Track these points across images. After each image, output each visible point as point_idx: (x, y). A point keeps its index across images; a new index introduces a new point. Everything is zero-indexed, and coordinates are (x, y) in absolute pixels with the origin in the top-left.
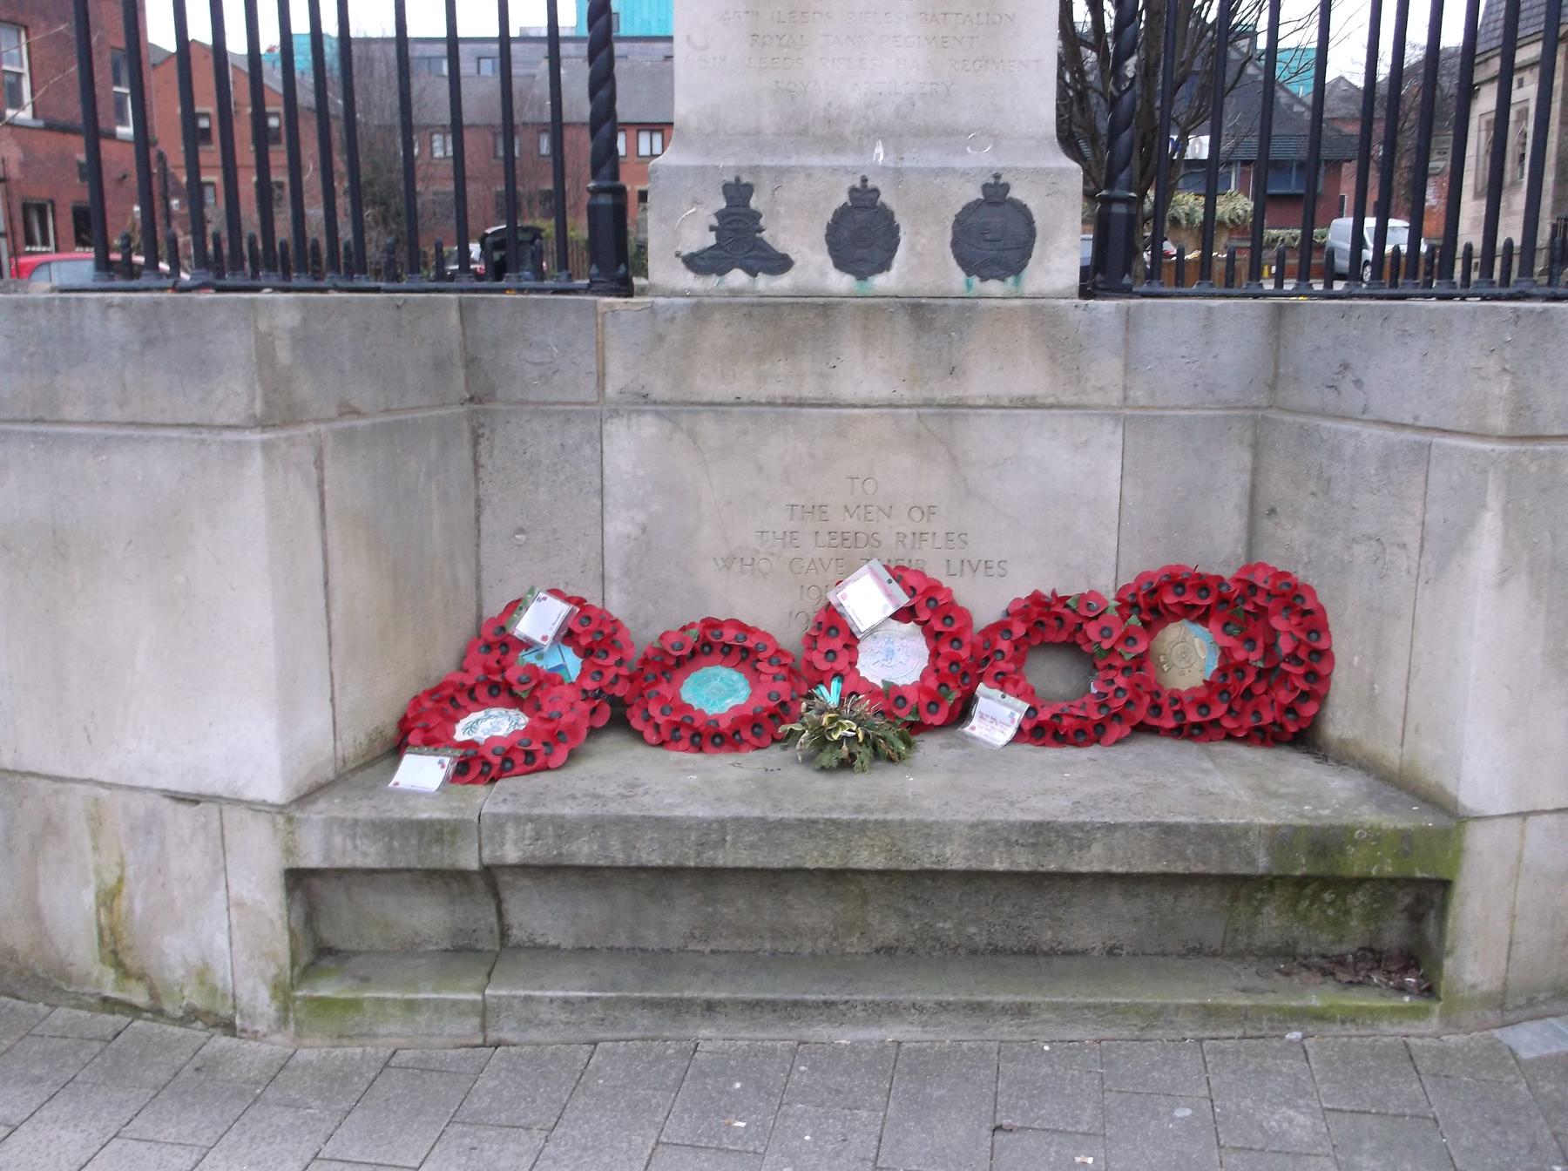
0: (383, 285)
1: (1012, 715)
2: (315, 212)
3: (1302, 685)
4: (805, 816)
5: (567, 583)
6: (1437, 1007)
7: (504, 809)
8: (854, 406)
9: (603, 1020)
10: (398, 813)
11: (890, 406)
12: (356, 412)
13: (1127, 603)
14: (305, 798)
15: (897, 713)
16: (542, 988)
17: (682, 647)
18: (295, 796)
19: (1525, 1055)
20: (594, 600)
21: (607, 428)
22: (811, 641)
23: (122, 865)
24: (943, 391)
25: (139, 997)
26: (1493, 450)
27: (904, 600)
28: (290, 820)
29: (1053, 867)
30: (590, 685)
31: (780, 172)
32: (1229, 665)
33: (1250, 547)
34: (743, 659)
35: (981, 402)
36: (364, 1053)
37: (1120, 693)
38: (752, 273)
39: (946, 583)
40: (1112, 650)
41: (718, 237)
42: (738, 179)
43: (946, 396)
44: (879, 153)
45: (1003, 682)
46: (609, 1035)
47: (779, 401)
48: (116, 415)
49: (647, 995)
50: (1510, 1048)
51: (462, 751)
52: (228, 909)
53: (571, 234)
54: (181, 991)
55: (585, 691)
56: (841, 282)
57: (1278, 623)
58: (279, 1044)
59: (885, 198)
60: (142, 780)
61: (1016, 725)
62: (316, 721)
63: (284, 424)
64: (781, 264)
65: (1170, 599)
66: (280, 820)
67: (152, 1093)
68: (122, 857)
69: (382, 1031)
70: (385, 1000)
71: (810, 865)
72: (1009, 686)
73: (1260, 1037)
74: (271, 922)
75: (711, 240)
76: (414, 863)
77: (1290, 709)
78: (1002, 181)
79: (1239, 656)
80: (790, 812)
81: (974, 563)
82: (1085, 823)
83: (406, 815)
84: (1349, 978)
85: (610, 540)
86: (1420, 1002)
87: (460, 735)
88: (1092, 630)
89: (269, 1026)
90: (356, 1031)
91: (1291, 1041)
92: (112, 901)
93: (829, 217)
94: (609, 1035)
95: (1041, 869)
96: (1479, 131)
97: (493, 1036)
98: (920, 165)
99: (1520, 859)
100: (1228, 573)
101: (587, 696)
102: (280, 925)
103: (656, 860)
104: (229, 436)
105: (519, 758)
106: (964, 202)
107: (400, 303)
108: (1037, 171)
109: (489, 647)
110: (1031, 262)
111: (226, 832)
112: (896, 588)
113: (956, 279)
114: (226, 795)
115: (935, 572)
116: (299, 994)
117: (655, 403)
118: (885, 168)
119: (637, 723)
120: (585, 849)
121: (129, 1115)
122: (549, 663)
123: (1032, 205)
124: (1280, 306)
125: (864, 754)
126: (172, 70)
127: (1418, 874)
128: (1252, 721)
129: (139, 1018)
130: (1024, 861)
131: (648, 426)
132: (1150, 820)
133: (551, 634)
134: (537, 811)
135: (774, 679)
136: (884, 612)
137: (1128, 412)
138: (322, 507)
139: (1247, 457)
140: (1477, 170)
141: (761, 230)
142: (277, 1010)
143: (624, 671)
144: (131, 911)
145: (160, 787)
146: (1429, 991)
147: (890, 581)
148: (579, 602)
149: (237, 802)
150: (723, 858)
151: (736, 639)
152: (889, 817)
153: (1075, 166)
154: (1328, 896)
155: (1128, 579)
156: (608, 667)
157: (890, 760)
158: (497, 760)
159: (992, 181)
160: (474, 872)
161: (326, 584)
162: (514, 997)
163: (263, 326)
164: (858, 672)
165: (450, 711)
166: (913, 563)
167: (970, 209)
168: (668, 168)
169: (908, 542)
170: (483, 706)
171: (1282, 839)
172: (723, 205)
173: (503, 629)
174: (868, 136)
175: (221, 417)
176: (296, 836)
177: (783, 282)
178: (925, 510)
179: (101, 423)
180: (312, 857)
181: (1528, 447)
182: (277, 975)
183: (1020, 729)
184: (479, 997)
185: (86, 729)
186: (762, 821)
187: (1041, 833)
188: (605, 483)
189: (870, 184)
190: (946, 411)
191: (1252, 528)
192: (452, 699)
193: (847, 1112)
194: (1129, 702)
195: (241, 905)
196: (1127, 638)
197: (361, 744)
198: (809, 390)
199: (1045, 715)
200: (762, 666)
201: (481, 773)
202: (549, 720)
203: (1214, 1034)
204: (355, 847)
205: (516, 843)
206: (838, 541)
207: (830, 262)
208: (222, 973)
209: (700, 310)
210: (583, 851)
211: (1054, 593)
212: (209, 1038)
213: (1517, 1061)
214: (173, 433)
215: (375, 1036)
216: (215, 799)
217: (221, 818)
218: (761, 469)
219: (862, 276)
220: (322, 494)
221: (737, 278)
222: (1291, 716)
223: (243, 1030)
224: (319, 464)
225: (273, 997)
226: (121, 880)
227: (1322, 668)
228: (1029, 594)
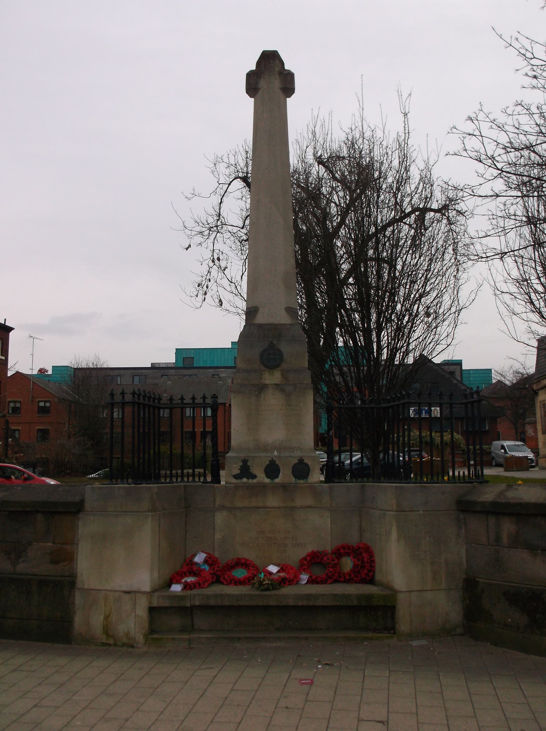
6: (395, 636)
13: (333, 553)
14: (154, 591)
17: (232, 564)
25: (111, 641)
28: (151, 596)
29: (311, 604)
30: (212, 572)
32: (355, 566)
35: (299, 507)
38: (248, 479)
40: (329, 563)
42: (245, 459)
44: (276, 453)
53: (174, 451)
56: (267, 481)
57: (364, 555)
58: (145, 649)
59: (277, 462)
60: (118, 589)
62: (156, 575)
64: (254, 477)
65: (342, 551)
66: (149, 596)
71: (260, 604)
75: (239, 472)
79: (356, 563)
88: (325, 559)
96: (541, 408)
97: (192, 646)
101: (211, 574)
104: (144, 513)
105: (197, 585)
106: (294, 463)
110: (309, 476)
113: (293, 480)
114: (137, 590)
118: (277, 456)
122: (203, 567)
124: (363, 485)
125: (271, 587)
130: (305, 603)
131: (225, 513)
133: (202, 561)
140: (542, 422)
141: (250, 470)
143: (219, 569)
148: (209, 554)
149: (139, 592)
150: (242, 603)
159: (300, 458)
167: (295, 465)
171: (360, 597)
173: (191, 560)
177: (255, 481)
180: (155, 604)
183: (308, 580)
187: (308, 597)
189: (274, 459)
194: (333, 574)
196: (333, 560)
198: (260, 504)
199: (314, 577)
200: (251, 568)
209: (237, 487)
210: (212, 602)
216: (135, 592)
220: (160, 526)
221: (245, 480)
223: (136, 647)
224: (160, 520)
226: (110, 613)
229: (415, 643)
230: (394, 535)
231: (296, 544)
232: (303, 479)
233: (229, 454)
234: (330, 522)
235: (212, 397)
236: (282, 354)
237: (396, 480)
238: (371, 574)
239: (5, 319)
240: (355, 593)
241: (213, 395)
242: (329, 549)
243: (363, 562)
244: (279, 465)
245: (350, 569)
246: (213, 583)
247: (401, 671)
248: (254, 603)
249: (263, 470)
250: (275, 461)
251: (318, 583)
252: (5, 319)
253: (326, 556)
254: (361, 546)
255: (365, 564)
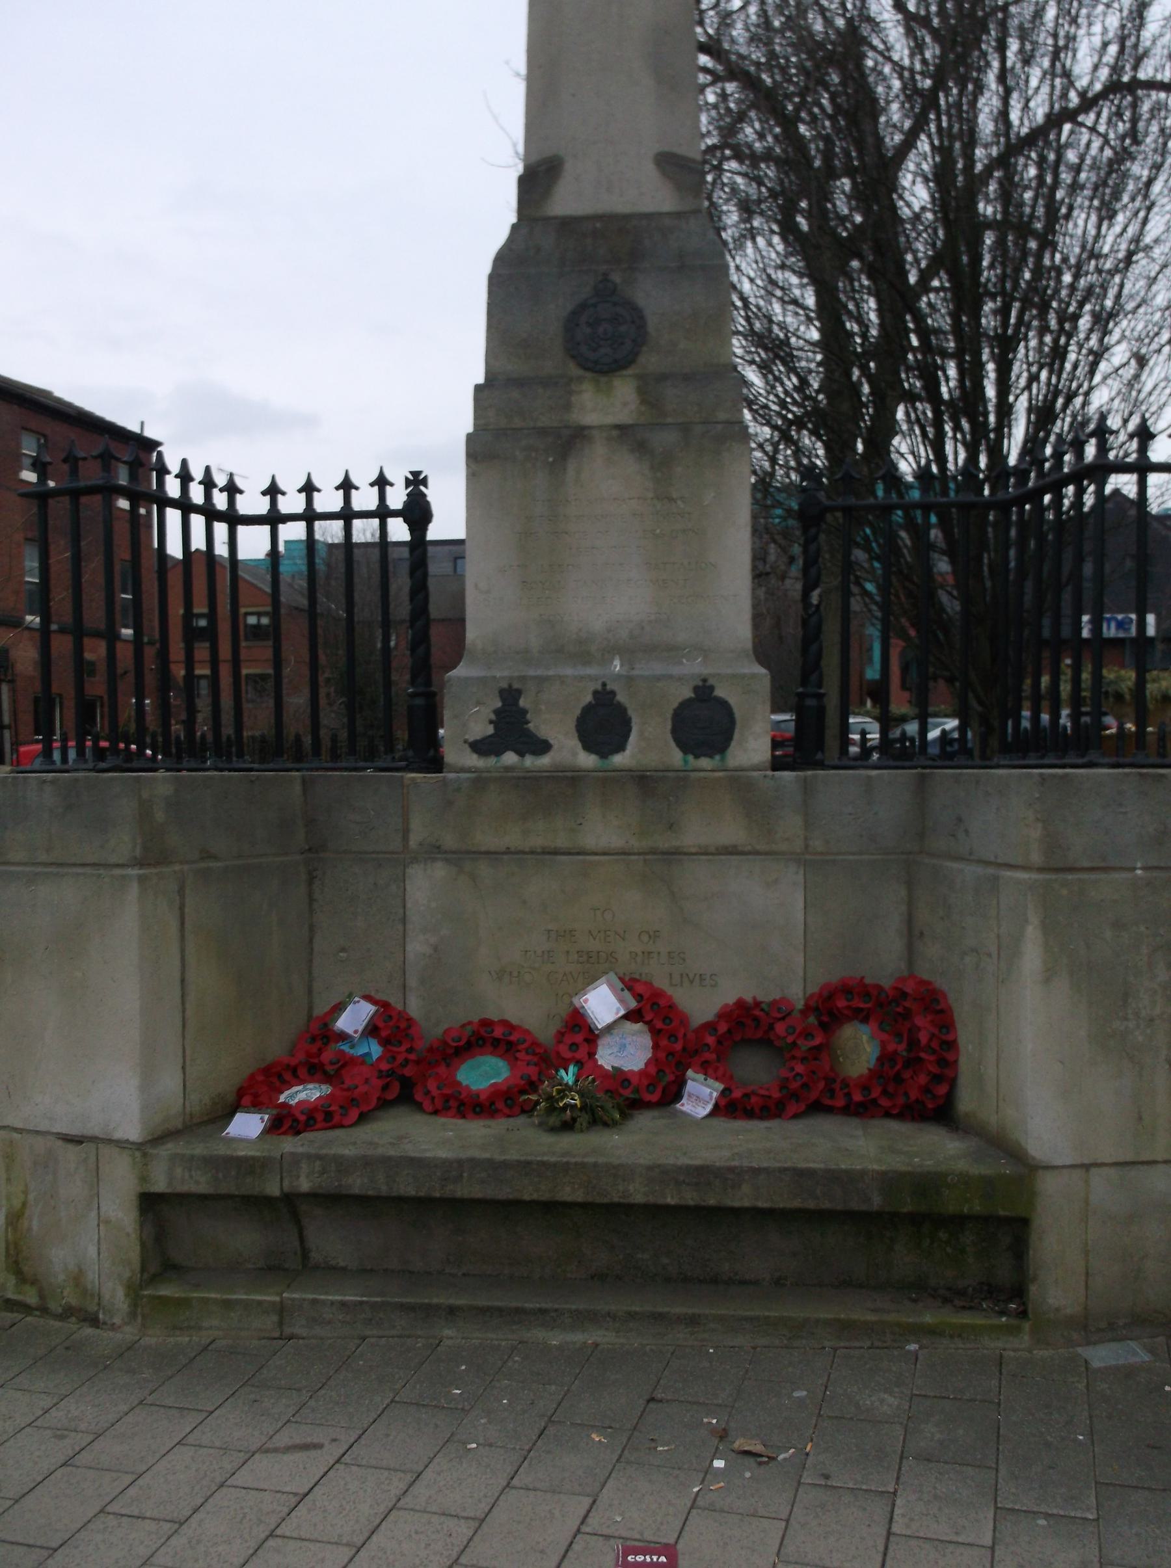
0: (256, 766)
1: (711, 1094)
2: (297, 701)
3: (934, 1069)
4: (522, 1158)
5: (377, 990)
6: (1027, 1326)
7: (300, 1150)
8: (596, 854)
9: (371, 1320)
10: (222, 1150)
11: (625, 853)
12: (214, 857)
13: (808, 1009)
14: (158, 1139)
15: (621, 1091)
16: (326, 1293)
18: (150, 1138)
19: (1096, 1364)
20: (396, 1002)
21: (409, 871)
22: (560, 1035)
23: (26, 1193)
24: (664, 842)
25: (31, 1298)
26: (1030, 879)
27: (633, 1004)
28: (145, 1155)
29: (712, 1202)
31: (541, 680)
32: (885, 1058)
33: (910, 963)
34: (507, 1051)
35: (693, 850)
36: (190, 1341)
37: (798, 1078)
38: (522, 754)
39: (670, 991)
40: (794, 1043)
41: (495, 728)
42: (510, 686)
43: (666, 846)
44: (617, 666)
45: (706, 1069)
46: (375, 1332)
47: (539, 850)
48: (43, 857)
49: (404, 1300)
50: (1086, 1361)
51: (278, 1110)
52: (98, 1225)
54: (62, 1292)
55: (381, 1071)
56: (587, 760)
57: (920, 1021)
58: (129, 1333)
59: (621, 698)
61: (713, 1101)
62: (170, 1083)
63: (157, 864)
64: (543, 747)
65: (841, 1003)
66: (138, 1154)
67: (31, 1362)
68: (26, 1186)
69: (205, 1324)
70: (208, 1299)
71: (526, 1197)
72: (710, 1071)
73: (883, 1348)
74: (128, 1235)
75: (490, 730)
76: (233, 1190)
77: (926, 1090)
78: (707, 684)
79: (891, 1047)
80: (513, 1155)
81: (691, 976)
82: (736, 1167)
83: (229, 1153)
84: (962, 1304)
85: (410, 956)
86: (1014, 1322)
87: (282, 1098)
88: (780, 1028)
89: (123, 1319)
90: (186, 1324)
91: (909, 1351)
92: (18, 1220)
93: (578, 712)
94: (375, 1332)
95: (703, 1204)
97: (288, 1331)
98: (647, 673)
99: (1087, 1202)
100: (887, 983)
101: (381, 1075)
102: (134, 1236)
103: (411, 1191)
104: (118, 872)
105: (320, 1117)
106: (680, 700)
107: (253, 779)
108: (734, 676)
109: (314, 1039)
110: (733, 744)
111: (100, 1165)
112: (627, 995)
113: (676, 757)
114: (101, 1136)
115: (661, 983)
116: (146, 1293)
117: (446, 852)
118: (619, 677)
119: (418, 1097)
120: (359, 1181)
121: (12, 1375)
122: (361, 1050)
123: (732, 701)
124: (923, 775)
125: (584, 1119)
126: (179, 570)
127: (1002, 1213)
128: (902, 1100)
129: (31, 1315)
130: (690, 1197)
131: (440, 871)
132: (786, 1165)
133: (361, 1029)
134: (324, 1152)
135: (528, 1064)
136: (617, 1013)
137: (808, 857)
138: (182, 924)
139: (903, 892)
141: (528, 722)
142: (129, 1306)
143: (412, 1057)
144: (29, 1229)
145: (55, 1131)
146: (1023, 1314)
147: (622, 990)
149: (110, 1141)
151: (503, 1034)
152: (586, 1160)
153: (763, 671)
154: (943, 1235)
155: (813, 989)
156: (399, 1053)
157: (606, 1125)
158: (303, 1118)
159: (700, 684)
160: (276, 1198)
161: (183, 981)
162: (304, 1300)
163: (145, 795)
164: (596, 1061)
165: (278, 1084)
166: (644, 976)
167: (685, 705)
168: (459, 678)
169: (639, 959)
170: (302, 1082)
171: (890, 1182)
172: (499, 704)
173: (326, 1025)
174: (609, 652)
175: (114, 859)
176: (149, 1167)
177: (545, 761)
178: (651, 933)
179: (34, 864)
180: (160, 1185)
181: (1061, 876)
182: (131, 1278)
184: (277, 1299)
185: (7, 1088)
186: (490, 1162)
187: (702, 1175)
188: (408, 913)
189: (608, 687)
190: (665, 857)
191: (910, 948)
192: (280, 1076)
193: (541, 1386)
194: (804, 1085)
195: (107, 1222)
196: (807, 1034)
197: (205, 1104)
198: (561, 842)
199: (737, 1094)
200: (520, 1055)
201: (291, 1127)
202: (348, 1090)
203: (847, 1344)
204: (191, 1177)
205: (307, 1177)
206: (585, 958)
207: (580, 746)
208: (92, 1277)
209: (480, 782)
210: (357, 1184)
211: (754, 998)
212: (79, 1329)
213: (1087, 1369)
214: (80, 870)
215: (200, 1328)
216: (93, 1139)
217: (97, 1154)
218: (524, 902)
219: (604, 755)
221: (510, 758)
222: (929, 1096)
223: (105, 1323)
225: (127, 1295)
226: (24, 1204)
227: (950, 1056)
228: (735, 1001)
229: (1102, 1356)
230: (1032, 957)
231: (682, 975)
232: (711, 756)
233: (461, 671)
234: (800, 904)
235: (408, 483)
236: (642, 318)
237: (1042, 757)
238: (942, 1090)
239: (142, 424)
240: (876, 1167)
241: (426, 478)
242: (797, 994)
243: (913, 1043)
244: (628, 706)
245: (869, 1070)
246: (384, 1104)
247: (1047, 1516)
248: (504, 1193)
249: (571, 724)
250: (613, 693)
251: (749, 1114)
252: (142, 424)
253: (783, 1018)
254: (909, 988)
255: (922, 1055)
